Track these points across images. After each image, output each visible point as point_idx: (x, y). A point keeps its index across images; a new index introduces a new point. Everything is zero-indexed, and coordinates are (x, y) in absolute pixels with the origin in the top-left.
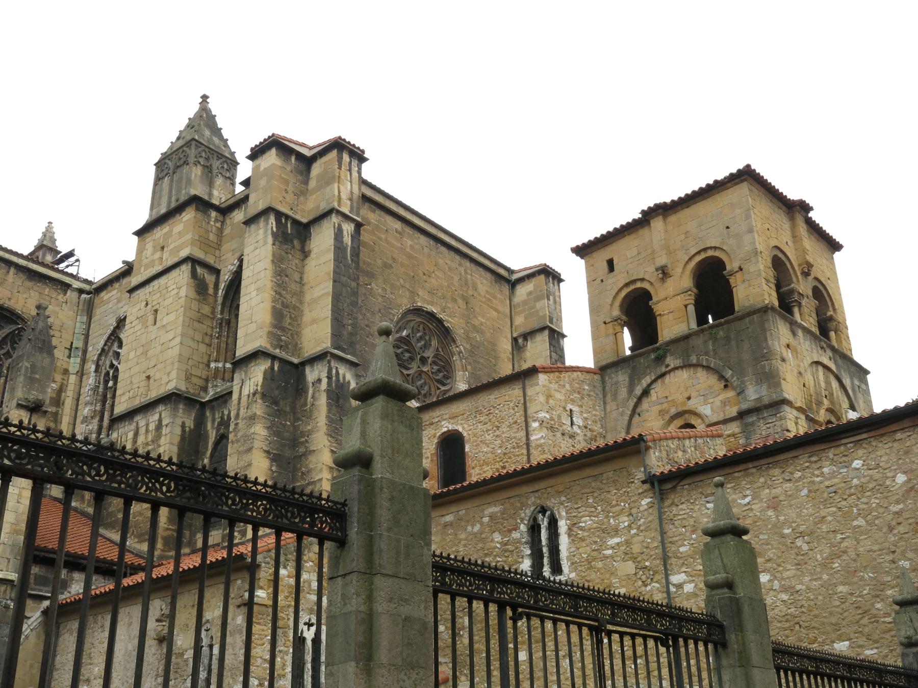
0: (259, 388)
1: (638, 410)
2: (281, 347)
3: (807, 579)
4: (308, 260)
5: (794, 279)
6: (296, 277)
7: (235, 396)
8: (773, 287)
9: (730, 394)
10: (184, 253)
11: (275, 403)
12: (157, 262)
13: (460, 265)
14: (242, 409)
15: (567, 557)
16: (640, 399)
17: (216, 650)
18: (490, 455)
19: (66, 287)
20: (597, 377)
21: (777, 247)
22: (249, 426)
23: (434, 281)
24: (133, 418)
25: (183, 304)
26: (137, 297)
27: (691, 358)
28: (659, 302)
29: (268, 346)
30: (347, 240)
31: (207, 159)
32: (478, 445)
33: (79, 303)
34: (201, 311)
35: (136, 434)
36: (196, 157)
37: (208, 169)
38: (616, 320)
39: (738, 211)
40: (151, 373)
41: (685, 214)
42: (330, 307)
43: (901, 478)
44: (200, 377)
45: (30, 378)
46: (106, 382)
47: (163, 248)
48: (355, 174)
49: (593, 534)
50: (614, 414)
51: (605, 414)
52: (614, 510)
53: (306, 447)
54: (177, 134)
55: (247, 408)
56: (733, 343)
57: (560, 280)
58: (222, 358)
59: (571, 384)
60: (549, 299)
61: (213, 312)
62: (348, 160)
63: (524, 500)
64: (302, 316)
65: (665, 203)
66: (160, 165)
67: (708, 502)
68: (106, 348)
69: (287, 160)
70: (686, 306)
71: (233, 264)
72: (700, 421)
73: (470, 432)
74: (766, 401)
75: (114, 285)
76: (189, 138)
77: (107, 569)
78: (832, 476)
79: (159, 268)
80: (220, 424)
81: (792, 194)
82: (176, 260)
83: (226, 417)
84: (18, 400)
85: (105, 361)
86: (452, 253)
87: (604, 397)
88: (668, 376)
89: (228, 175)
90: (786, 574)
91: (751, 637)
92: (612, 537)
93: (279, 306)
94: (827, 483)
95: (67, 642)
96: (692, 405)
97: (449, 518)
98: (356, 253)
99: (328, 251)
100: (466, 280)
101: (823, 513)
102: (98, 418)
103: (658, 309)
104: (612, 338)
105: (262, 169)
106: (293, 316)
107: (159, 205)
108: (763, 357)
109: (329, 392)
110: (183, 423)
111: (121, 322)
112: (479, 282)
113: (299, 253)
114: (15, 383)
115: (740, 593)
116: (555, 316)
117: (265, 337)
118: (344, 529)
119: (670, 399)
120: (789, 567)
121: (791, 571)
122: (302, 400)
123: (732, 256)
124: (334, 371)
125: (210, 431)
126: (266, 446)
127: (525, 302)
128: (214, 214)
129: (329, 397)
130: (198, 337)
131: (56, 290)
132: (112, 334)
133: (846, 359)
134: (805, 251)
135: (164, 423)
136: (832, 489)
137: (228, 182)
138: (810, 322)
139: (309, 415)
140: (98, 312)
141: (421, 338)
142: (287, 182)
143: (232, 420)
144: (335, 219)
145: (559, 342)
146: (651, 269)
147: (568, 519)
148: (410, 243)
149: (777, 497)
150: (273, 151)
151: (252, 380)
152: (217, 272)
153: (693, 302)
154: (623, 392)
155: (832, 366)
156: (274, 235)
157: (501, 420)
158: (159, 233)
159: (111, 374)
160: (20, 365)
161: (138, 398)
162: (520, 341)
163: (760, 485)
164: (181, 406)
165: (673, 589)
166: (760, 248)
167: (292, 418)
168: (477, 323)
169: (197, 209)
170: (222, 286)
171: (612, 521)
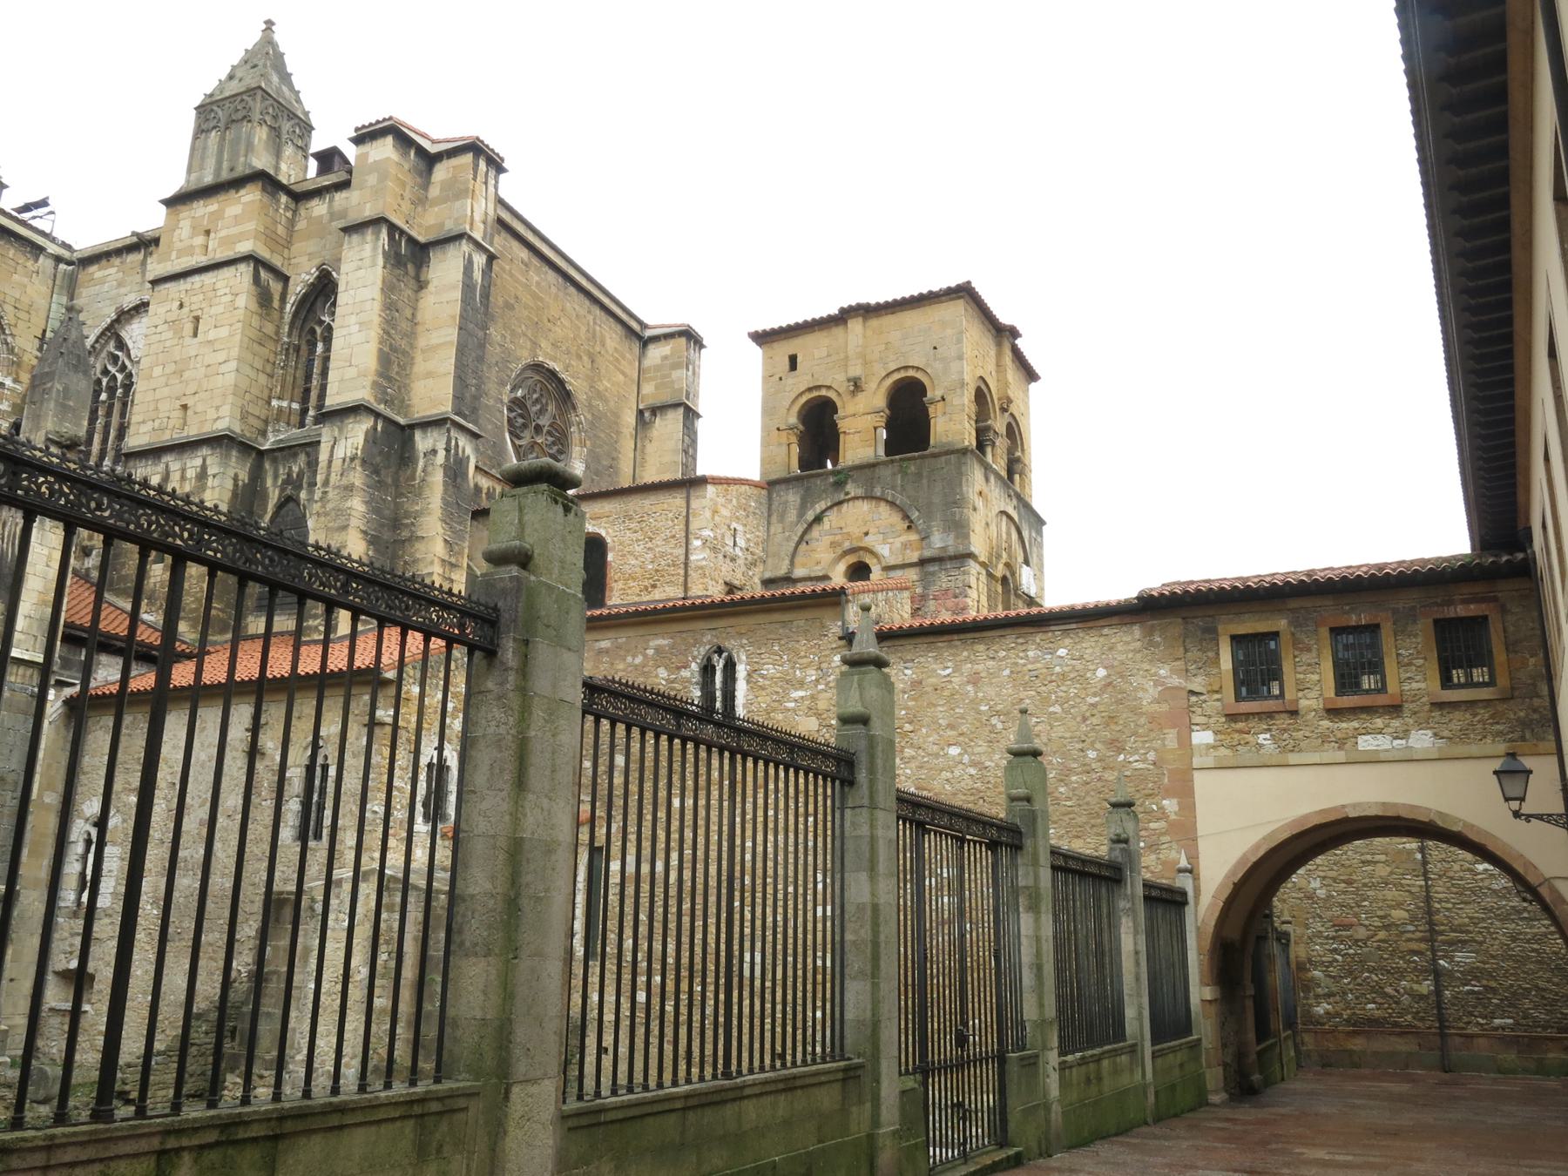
1: (807, 537)
3: (997, 757)
4: (423, 293)
6: (408, 312)
9: (913, 537)
10: (244, 247)
11: (376, 472)
12: (198, 250)
13: (589, 312)
14: (333, 475)
16: (810, 526)
17: (332, 772)
18: (638, 569)
19: (38, 250)
20: (764, 492)
21: (981, 378)
22: (345, 498)
24: (159, 458)
25: (242, 318)
26: (165, 292)
28: (845, 417)
29: (372, 400)
30: (477, 276)
31: (275, 117)
32: (624, 556)
33: (55, 276)
37: (275, 131)
39: (949, 332)
40: (190, 402)
41: (888, 321)
42: (453, 361)
43: (1101, 673)
44: (259, 418)
46: (97, 394)
47: (208, 233)
48: (491, 189)
49: (776, 683)
50: (779, 537)
51: (768, 536)
52: (800, 661)
54: (228, 69)
56: (925, 481)
57: (702, 346)
58: (288, 395)
59: (738, 500)
60: (688, 369)
61: (277, 333)
62: (485, 169)
63: (698, 637)
64: (412, 364)
65: (868, 304)
66: (204, 110)
69: (405, 155)
70: (875, 428)
71: (308, 273)
72: (875, 561)
74: (951, 551)
76: (250, 81)
77: (129, 650)
78: (1036, 660)
80: (288, 481)
81: (1004, 318)
84: (47, 433)
86: (582, 296)
87: (769, 516)
88: (845, 505)
89: (300, 143)
90: (977, 750)
91: (1041, 842)
92: (796, 689)
93: (386, 349)
94: (1030, 667)
95: (98, 739)
96: (869, 542)
97: (605, 644)
98: (486, 295)
99: (454, 287)
100: (594, 331)
103: (842, 425)
104: (785, 448)
105: (371, 160)
107: (202, 168)
108: (955, 503)
109: (446, 468)
113: (412, 282)
114: (40, 409)
115: (1037, 807)
116: (692, 391)
117: (368, 389)
118: (852, 772)
119: (844, 531)
120: (981, 743)
121: (982, 747)
122: (409, 472)
123: (936, 382)
124: (453, 442)
125: (271, 489)
127: (657, 368)
128: (284, 199)
129: (446, 475)
130: (258, 364)
131: (24, 253)
132: (107, 329)
133: (1025, 505)
134: (1007, 385)
135: (210, 471)
137: (300, 153)
138: (1000, 466)
139: (418, 492)
141: (537, 400)
142: (403, 185)
143: (319, 485)
144: (465, 247)
145: (693, 424)
147: (747, 664)
150: (389, 140)
151: (350, 441)
154: (792, 515)
155: (1016, 518)
157: (656, 532)
158: (202, 210)
159: (104, 384)
160: (49, 385)
162: (647, 414)
164: (234, 453)
166: (967, 378)
168: (601, 388)
169: (264, 190)
170: (291, 299)
171: (798, 672)
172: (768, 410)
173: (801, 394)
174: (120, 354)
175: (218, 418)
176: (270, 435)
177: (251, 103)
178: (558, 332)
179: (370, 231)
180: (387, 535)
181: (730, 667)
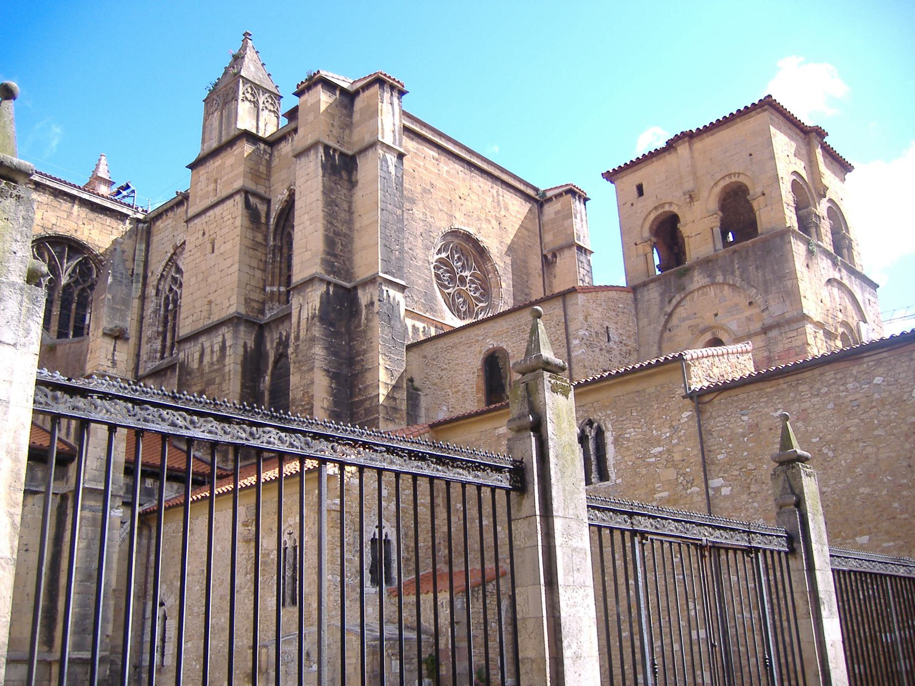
0: (317, 312)
1: (669, 326)
2: (334, 273)
4: (354, 191)
5: (812, 203)
7: (294, 319)
8: (793, 210)
10: (238, 185)
12: (211, 194)
14: (301, 331)
15: (614, 464)
21: (795, 173)
23: (469, 203)
27: (718, 277)
29: (323, 272)
34: (256, 239)
35: (202, 355)
36: (244, 94)
38: (646, 242)
40: (212, 297)
41: (708, 141)
44: (258, 301)
45: (113, 309)
46: (167, 305)
52: (656, 422)
53: (362, 366)
55: (307, 331)
57: (586, 200)
58: (277, 282)
67: (743, 415)
68: (164, 273)
73: (514, 349)
75: (169, 214)
79: (213, 199)
80: (279, 344)
81: (809, 122)
82: (229, 191)
83: (284, 338)
85: (164, 285)
93: (331, 235)
94: (850, 398)
101: (847, 424)
102: (161, 338)
104: (642, 258)
106: (344, 243)
110: (245, 344)
111: (179, 249)
112: (510, 203)
113: (346, 183)
122: (356, 322)
126: (325, 365)
130: (254, 263)
132: (170, 260)
135: (228, 344)
136: (856, 403)
138: (827, 243)
140: (155, 239)
146: (679, 193)
148: (446, 168)
149: (806, 410)
150: (320, 86)
151: (310, 305)
152: (268, 202)
153: (719, 225)
154: (655, 310)
156: (324, 167)
158: (213, 165)
160: (103, 296)
161: (202, 321)
163: (790, 399)
165: (711, 492)
167: (347, 339)
170: (273, 214)
172: (624, 231)
173: (649, 214)
174: (178, 276)
175: (230, 305)
176: (267, 312)
177: (261, 95)
178: (468, 205)
179: (312, 152)
180: (345, 370)
181: (600, 433)
